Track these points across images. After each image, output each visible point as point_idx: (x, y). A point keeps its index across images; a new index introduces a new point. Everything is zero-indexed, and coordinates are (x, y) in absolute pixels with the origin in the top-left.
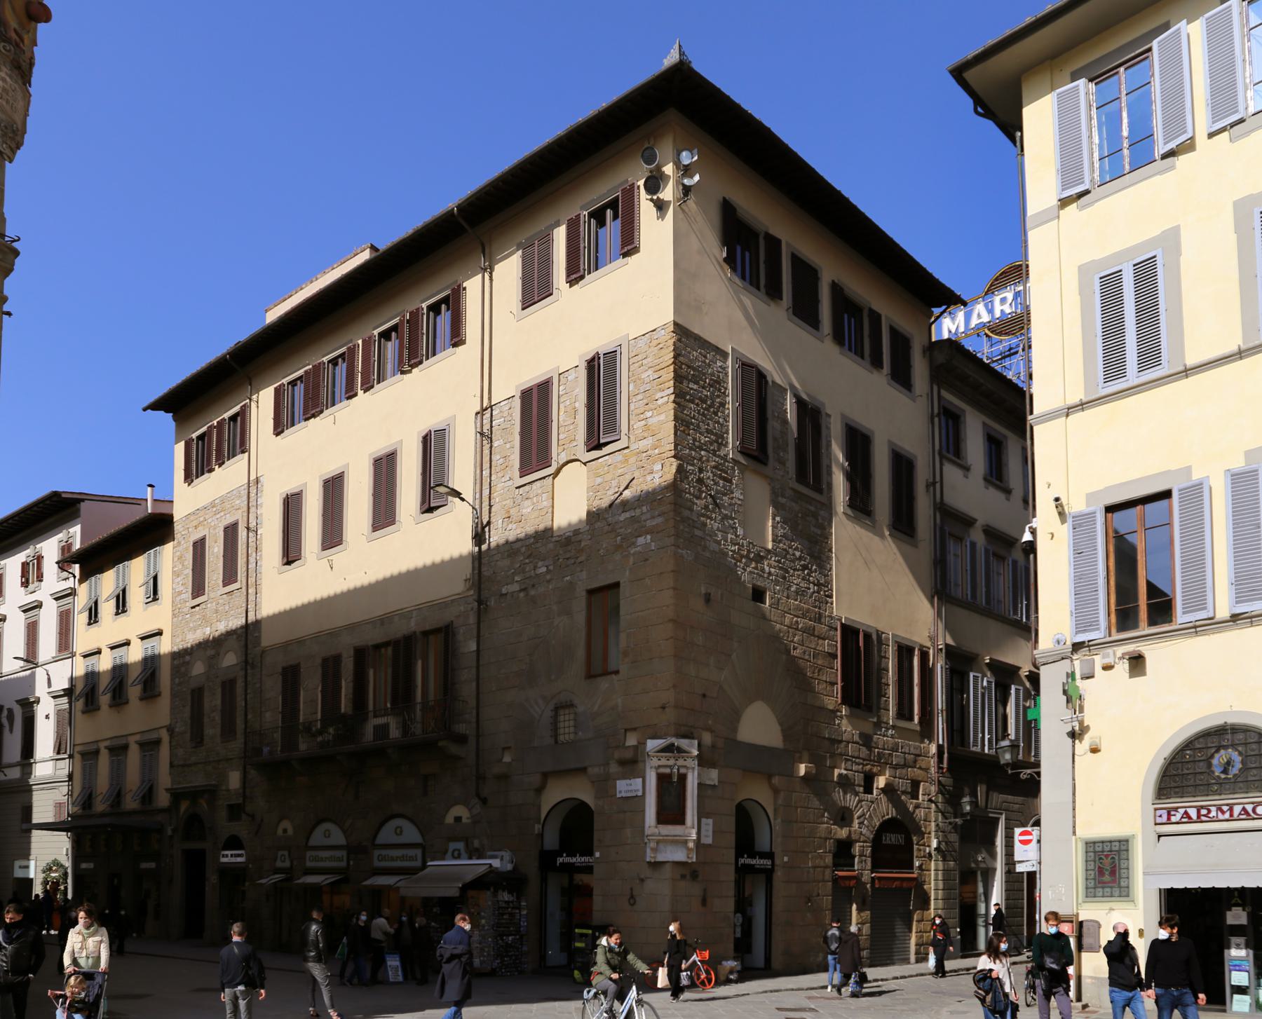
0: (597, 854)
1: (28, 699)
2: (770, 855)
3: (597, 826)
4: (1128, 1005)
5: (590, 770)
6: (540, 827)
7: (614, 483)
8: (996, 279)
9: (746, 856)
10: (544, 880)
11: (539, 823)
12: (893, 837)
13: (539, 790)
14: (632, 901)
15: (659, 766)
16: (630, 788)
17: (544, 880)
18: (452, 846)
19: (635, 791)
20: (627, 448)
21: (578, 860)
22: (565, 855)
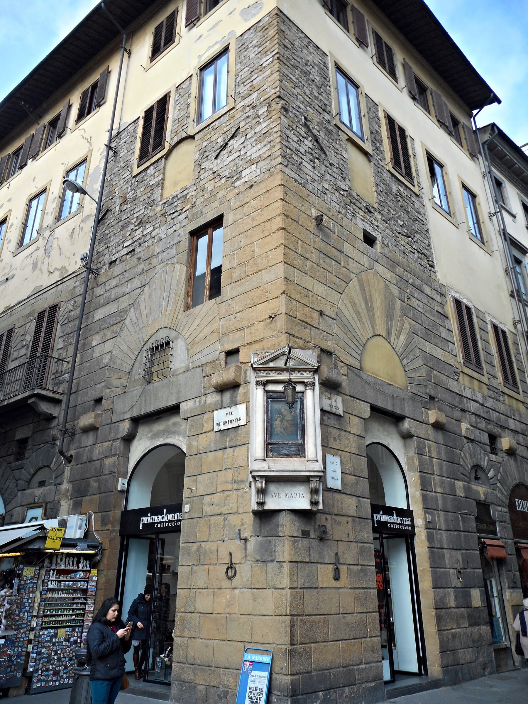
0: (186, 508)
1: (122, 511)
2: (407, 513)
3: (188, 470)
4: (35, 503)
5: (184, 407)
6: (126, 482)
7: (220, 140)
8: (365, 428)
9: (381, 513)
10: (124, 549)
11: (124, 477)
12: (110, 612)
13: (129, 439)
14: (231, 573)
15: (268, 382)
16: (230, 418)
17: (124, 549)
18: (31, 513)
19: (237, 420)
20: (234, 108)
21: (164, 518)
22: (149, 514)
